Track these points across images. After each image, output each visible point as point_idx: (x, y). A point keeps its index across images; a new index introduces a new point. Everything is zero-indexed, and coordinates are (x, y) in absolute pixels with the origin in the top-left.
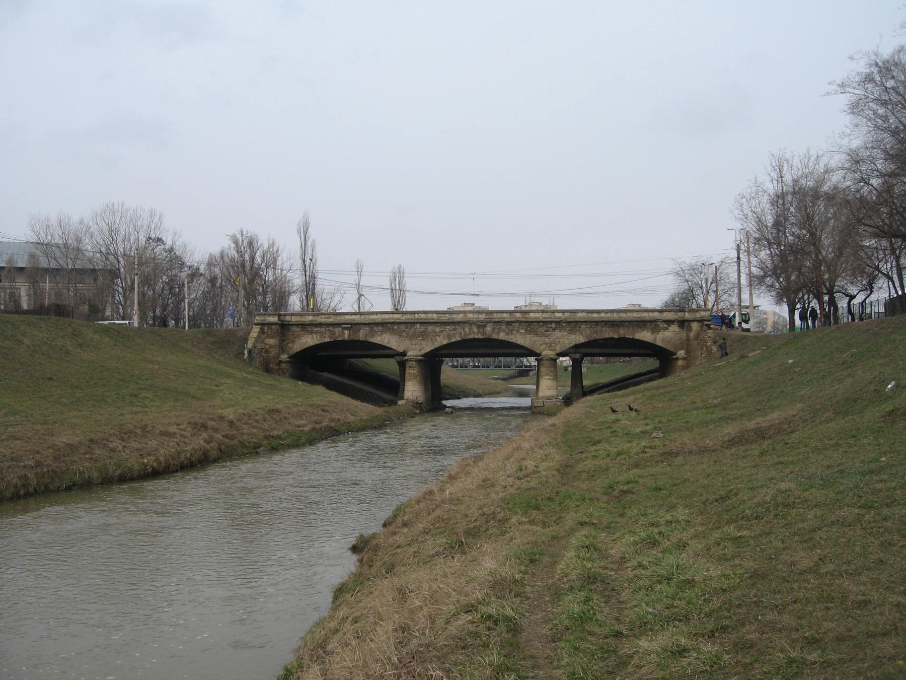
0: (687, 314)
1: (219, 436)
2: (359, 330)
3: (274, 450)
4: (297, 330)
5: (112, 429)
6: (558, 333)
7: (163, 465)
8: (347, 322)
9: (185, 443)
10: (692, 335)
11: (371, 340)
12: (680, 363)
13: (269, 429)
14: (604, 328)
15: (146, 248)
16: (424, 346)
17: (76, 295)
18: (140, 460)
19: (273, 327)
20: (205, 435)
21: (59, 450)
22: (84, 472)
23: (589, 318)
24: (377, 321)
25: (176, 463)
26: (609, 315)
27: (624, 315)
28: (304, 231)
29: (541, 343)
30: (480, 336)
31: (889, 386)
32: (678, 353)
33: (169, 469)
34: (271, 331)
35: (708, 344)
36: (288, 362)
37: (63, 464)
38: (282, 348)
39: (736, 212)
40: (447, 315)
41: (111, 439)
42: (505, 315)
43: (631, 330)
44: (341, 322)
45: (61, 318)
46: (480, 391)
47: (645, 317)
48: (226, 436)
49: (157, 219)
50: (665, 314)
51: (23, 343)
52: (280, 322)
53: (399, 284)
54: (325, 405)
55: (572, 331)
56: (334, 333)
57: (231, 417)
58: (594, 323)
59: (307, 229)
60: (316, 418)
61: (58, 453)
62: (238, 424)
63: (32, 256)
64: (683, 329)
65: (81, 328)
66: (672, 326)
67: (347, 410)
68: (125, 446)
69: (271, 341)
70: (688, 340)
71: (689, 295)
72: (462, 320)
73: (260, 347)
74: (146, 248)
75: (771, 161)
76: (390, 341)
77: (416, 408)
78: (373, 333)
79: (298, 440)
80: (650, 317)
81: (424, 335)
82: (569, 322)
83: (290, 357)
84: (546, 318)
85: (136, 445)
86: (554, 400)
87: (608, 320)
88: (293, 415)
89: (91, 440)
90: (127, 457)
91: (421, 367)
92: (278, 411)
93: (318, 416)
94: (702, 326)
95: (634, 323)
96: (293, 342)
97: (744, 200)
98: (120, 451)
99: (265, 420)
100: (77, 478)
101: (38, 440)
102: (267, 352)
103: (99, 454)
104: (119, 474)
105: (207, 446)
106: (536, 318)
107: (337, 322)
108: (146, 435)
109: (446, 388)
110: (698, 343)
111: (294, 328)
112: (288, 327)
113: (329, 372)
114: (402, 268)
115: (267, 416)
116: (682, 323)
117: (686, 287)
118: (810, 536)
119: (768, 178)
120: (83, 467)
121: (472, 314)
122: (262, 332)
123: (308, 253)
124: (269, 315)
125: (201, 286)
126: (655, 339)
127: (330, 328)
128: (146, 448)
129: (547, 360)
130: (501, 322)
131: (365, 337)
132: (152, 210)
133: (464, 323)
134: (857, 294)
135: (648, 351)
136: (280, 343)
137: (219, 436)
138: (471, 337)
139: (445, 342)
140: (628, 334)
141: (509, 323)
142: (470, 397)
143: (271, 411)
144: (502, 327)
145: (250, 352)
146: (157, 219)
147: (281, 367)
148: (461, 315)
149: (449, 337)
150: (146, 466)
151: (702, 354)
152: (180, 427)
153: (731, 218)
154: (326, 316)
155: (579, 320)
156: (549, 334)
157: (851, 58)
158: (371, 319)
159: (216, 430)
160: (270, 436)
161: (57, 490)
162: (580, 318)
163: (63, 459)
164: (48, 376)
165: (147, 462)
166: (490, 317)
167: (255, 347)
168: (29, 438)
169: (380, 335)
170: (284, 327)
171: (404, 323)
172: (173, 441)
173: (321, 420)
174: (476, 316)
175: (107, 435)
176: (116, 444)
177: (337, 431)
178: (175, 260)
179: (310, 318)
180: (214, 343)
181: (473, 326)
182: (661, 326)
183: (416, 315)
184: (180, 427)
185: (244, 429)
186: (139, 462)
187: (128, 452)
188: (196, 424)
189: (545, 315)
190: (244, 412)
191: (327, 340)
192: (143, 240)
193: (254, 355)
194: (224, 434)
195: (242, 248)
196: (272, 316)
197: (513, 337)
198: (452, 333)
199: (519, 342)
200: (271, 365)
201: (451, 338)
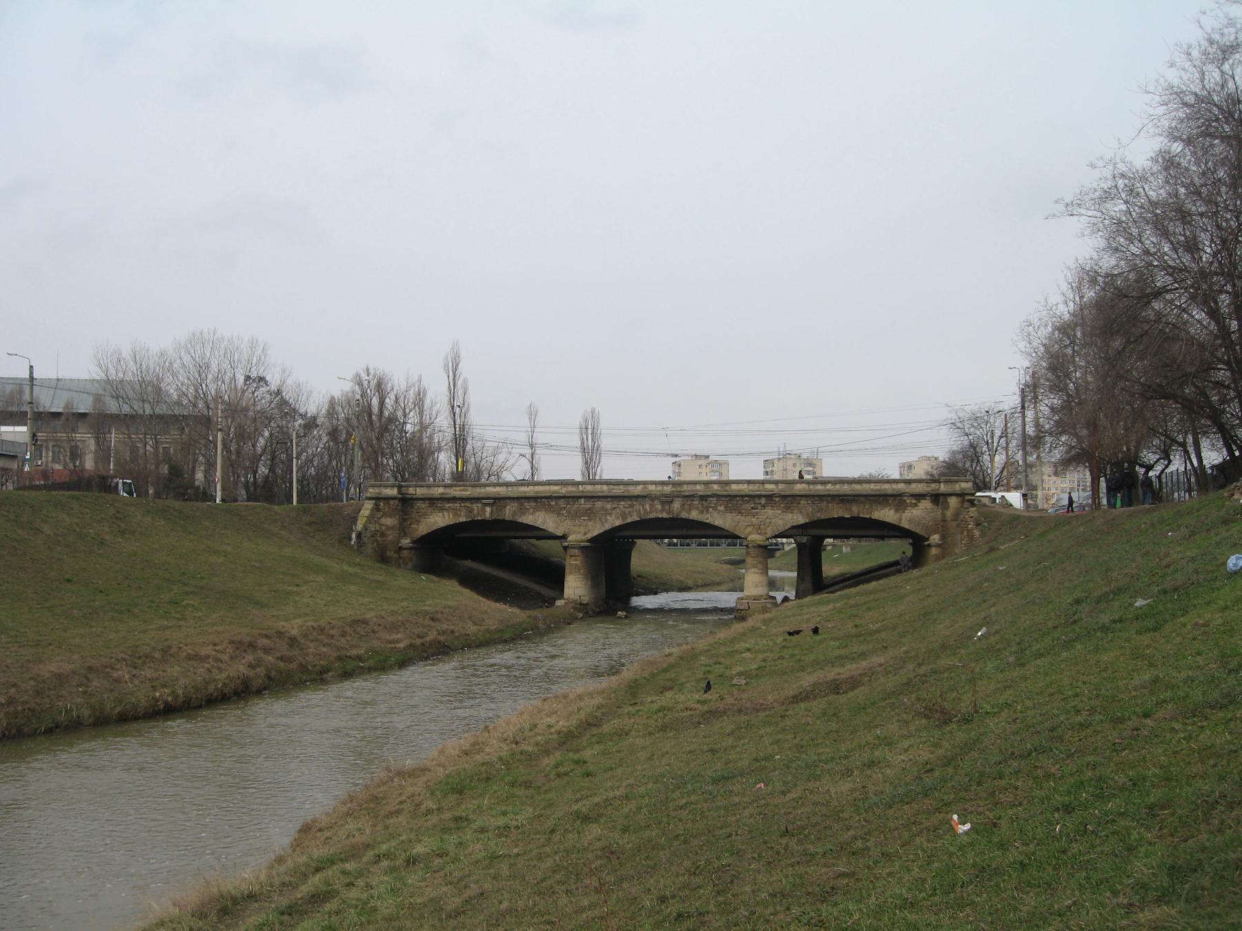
0: (942, 485)
1: (270, 659)
2: (505, 507)
3: (347, 675)
4: (423, 506)
5: (122, 652)
6: (769, 511)
7: (181, 699)
8: (490, 496)
9: (219, 669)
10: (949, 513)
11: (520, 520)
12: (934, 551)
13: (347, 647)
14: (830, 505)
15: (243, 392)
16: (590, 527)
17: (156, 449)
18: (151, 694)
19: (392, 502)
20: (250, 658)
21: (44, 682)
22: (71, 710)
23: (810, 490)
24: (528, 495)
25: (199, 696)
26: (838, 487)
27: (857, 487)
28: (453, 368)
29: (746, 524)
30: (665, 515)
31: (979, 634)
32: (931, 538)
33: (189, 704)
34: (389, 508)
35: (970, 526)
36: (411, 549)
37: (47, 700)
38: (403, 530)
39: (1022, 345)
40: (622, 487)
41: (118, 666)
42: (698, 487)
43: (867, 506)
44: (481, 496)
45: (103, 494)
46: (690, 582)
47: (886, 489)
48: (282, 659)
49: (259, 352)
50: (914, 486)
51: (43, 532)
52: (400, 496)
53: (592, 434)
54: (436, 612)
55: (787, 509)
56: (471, 511)
57: (294, 632)
58: (817, 498)
59: (457, 365)
60: (420, 629)
61: (41, 685)
62: (303, 641)
63: (98, 399)
64: (938, 505)
65: (128, 508)
66: (923, 501)
67: (470, 618)
68: (134, 676)
69: (389, 521)
70: (944, 521)
71: (972, 453)
72: (642, 494)
73: (373, 529)
74: (243, 392)
75: (1065, 276)
76: (545, 521)
77: (579, 611)
78: (523, 511)
79: (385, 661)
80: (893, 490)
81: (590, 514)
82: (784, 497)
83: (414, 542)
84: (753, 491)
85: (148, 673)
86: (763, 601)
87: (836, 493)
88: (385, 627)
89: (90, 669)
90: (135, 689)
91: (586, 556)
92: (365, 622)
93: (424, 626)
94: (963, 502)
95: (872, 498)
96: (418, 522)
97: (1031, 328)
98: (126, 682)
99: (344, 634)
100: (62, 718)
101: (19, 669)
102: (383, 535)
103: (96, 687)
104: (118, 713)
105: (251, 673)
106: (739, 491)
107: (475, 495)
108: (167, 660)
109: (639, 579)
110: (958, 526)
111: (419, 504)
112: (411, 502)
113: (473, 560)
114: (597, 412)
115: (348, 629)
116: (937, 498)
117: (966, 443)
119: (1060, 299)
120: (72, 703)
121: (654, 486)
122: (377, 508)
123: (458, 397)
124: (386, 487)
125: (320, 440)
126: (901, 519)
127: (466, 504)
128: (164, 677)
129: (754, 547)
130: (692, 496)
131: (513, 516)
132: (253, 338)
133: (645, 497)
134: (1156, 462)
135: (896, 533)
136: (401, 524)
137: (270, 659)
138: (653, 516)
139: (618, 523)
140: (863, 513)
141: (703, 498)
142: (673, 590)
143: (357, 622)
144: (695, 502)
145: (359, 536)
146: (259, 352)
147: (402, 555)
148: (640, 487)
149: (624, 516)
150: (158, 701)
151: (962, 540)
152: (217, 648)
153: (1015, 353)
154: (462, 488)
155: (798, 493)
156: (757, 513)
157: (1093, 166)
158: (520, 492)
159: (267, 651)
160: (346, 656)
161: (34, 734)
162: (800, 491)
163: (47, 693)
164: (67, 576)
165: (160, 696)
166: (679, 489)
167: (366, 529)
168: (7, 666)
169: (532, 514)
170: (406, 502)
171: (564, 497)
172: (203, 667)
173: (426, 633)
174: (659, 488)
175: (113, 660)
176: (123, 672)
177: (448, 647)
178: (285, 408)
179: (441, 490)
180: (311, 524)
181: (656, 502)
182: (908, 501)
183: (580, 486)
184: (217, 648)
185: (309, 648)
186: (149, 697)
187: (136, 682)
188: (241, 643)
189: (751, 487)
190: (314, 624)
191: (463, 519)
192: (241, 379)
193: (365, 539)
194: (278, 655)
195: (369, 391)
197: (708, 516)
198: (627, 510)
199: (716, 523)
200: (388, 553)
201: (627, 518)
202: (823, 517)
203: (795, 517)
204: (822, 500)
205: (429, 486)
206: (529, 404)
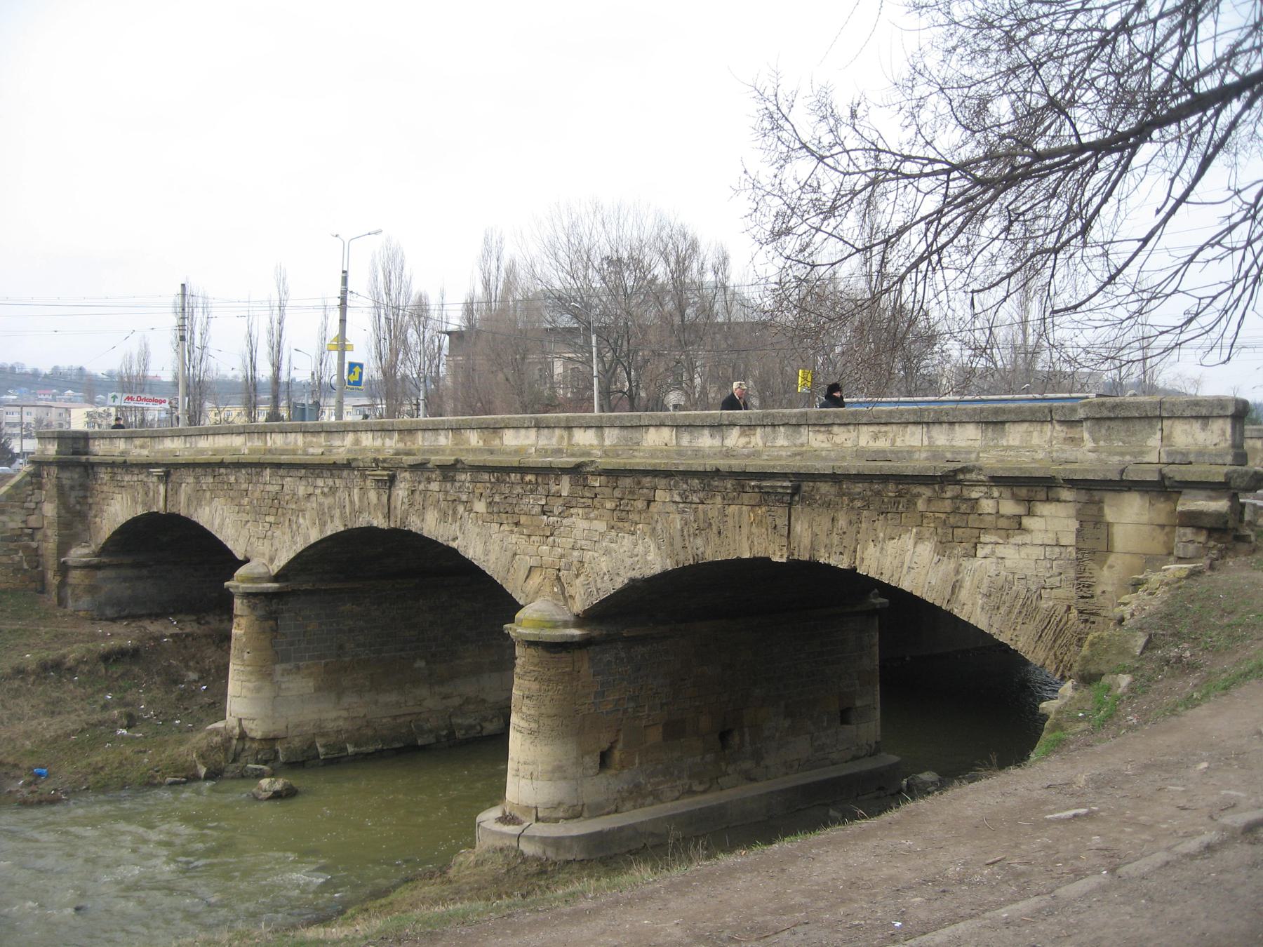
6: (581, 525)
14: (732, 509)
47: (910, 451)
50: (1015, 435)
55: (621, 517)
66: (1045, 509)
80: (935, 454)
82: (613, 474)
95: (858, 488)
118: (98, 776)
126: (956, 587)
158: (164, 453)
182: (987, 506)
196: (706, 432)
202: (709, 557)
203: (640, 549)
204: (709, 490)
205: (329, 431)
206: (749, 112)
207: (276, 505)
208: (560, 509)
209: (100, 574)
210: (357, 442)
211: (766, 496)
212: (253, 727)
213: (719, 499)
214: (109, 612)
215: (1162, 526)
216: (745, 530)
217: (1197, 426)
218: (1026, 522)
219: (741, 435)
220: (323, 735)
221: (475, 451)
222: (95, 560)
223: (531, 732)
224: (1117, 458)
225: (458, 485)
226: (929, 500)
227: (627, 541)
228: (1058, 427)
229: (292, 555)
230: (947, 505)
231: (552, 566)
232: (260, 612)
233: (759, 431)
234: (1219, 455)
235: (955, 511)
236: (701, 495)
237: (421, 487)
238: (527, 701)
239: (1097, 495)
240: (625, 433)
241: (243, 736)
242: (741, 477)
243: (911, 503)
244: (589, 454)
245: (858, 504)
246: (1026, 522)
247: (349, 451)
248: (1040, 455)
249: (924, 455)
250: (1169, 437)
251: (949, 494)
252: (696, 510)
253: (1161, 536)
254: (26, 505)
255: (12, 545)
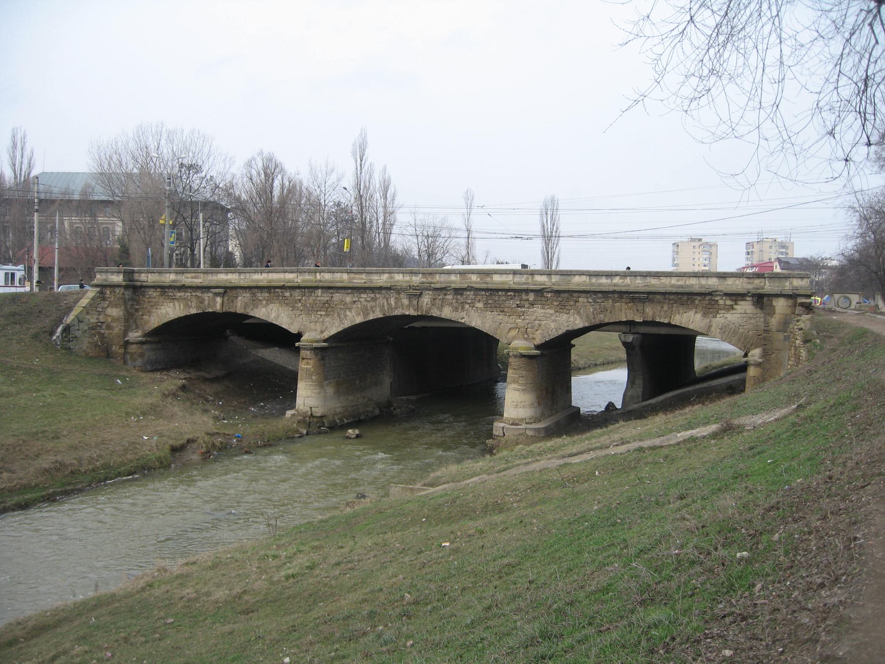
14: (617, 304)
66: (742, 303)
80: (702, 286)
82: (558, 292)
95: (672, 297)
158: (254, 281)
182: (721, 302)
196: (604, 277)
203: (572, 319)
204: (607, 298)
207: (328, 307)
208: (528, 305)
209: (145, 347)
210: (391, 278)
211: (633, 300)
212: (317, 410)
213: (610, 301)
214: (149, 367)
215: (790, 306)
216: (623, 312)
217: (800, 280)
218: (735, 307)
219: (620, 279)
220: (336, 414)
221: (476, 283)
222: (144, 339)
223: (523, 390)
224: (777, 288)
225: (465, 296)
226: (700, 300)
227: (565, 317)
228: (745, 279)
229: (340, 329)
230: (707, 302)
231: (524, 327)
232: (320, 357)
233: (628, 278)
234: (807, 287)
235: (710, 304)
236: (603, 299)
237: (441, 297)
238: (521, 378)
239: (771, 298)
240: (563, 277)
241: (312, 416)
242: (621, 294)
243: (693, 301)
244: (544, 285)
245: (671, 302)
246: (735, 307)
247: (386, 282)
248: (739, 287)
249: (697, 287)
250: (792, 282)
251: (707, 299)
252: (600, 305)
253: (790, 309)
254: (98, 309)
255: (93, 332)
